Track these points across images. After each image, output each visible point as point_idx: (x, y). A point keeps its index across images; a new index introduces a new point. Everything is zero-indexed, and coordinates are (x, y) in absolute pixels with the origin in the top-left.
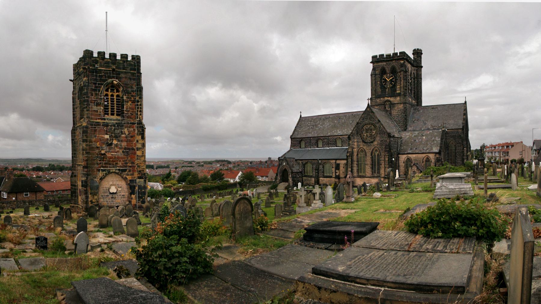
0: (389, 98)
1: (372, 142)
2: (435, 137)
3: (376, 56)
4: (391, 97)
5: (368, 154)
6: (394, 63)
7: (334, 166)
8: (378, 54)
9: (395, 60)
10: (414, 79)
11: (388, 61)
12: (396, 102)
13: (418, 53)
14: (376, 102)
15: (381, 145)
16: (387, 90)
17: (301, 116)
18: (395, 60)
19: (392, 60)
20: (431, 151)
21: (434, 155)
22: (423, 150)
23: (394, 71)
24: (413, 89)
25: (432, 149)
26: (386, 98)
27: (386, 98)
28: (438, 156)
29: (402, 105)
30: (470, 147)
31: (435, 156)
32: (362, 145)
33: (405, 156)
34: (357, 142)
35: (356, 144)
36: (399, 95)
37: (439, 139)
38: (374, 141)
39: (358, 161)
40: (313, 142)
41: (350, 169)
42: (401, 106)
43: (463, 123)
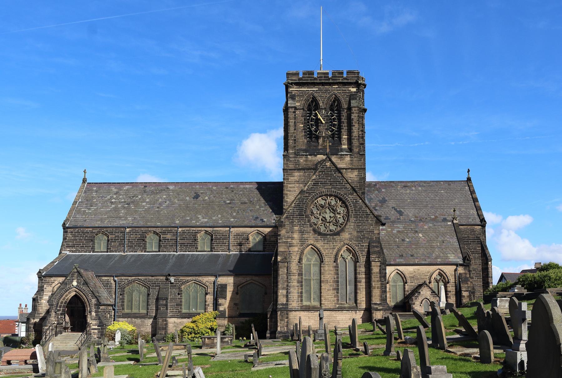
1: (338, 234)
5: (326, 259)
7: (210, 290)
11: (323, 84)
14: (297, 163)
17: (84, 181)
19: (330, 84)
20: (447, 261)
28: (461, 270)
29: (356, 173)
33: (393, 268)
38: (342, 230)
39: (300, 274)
41: (284, 292)
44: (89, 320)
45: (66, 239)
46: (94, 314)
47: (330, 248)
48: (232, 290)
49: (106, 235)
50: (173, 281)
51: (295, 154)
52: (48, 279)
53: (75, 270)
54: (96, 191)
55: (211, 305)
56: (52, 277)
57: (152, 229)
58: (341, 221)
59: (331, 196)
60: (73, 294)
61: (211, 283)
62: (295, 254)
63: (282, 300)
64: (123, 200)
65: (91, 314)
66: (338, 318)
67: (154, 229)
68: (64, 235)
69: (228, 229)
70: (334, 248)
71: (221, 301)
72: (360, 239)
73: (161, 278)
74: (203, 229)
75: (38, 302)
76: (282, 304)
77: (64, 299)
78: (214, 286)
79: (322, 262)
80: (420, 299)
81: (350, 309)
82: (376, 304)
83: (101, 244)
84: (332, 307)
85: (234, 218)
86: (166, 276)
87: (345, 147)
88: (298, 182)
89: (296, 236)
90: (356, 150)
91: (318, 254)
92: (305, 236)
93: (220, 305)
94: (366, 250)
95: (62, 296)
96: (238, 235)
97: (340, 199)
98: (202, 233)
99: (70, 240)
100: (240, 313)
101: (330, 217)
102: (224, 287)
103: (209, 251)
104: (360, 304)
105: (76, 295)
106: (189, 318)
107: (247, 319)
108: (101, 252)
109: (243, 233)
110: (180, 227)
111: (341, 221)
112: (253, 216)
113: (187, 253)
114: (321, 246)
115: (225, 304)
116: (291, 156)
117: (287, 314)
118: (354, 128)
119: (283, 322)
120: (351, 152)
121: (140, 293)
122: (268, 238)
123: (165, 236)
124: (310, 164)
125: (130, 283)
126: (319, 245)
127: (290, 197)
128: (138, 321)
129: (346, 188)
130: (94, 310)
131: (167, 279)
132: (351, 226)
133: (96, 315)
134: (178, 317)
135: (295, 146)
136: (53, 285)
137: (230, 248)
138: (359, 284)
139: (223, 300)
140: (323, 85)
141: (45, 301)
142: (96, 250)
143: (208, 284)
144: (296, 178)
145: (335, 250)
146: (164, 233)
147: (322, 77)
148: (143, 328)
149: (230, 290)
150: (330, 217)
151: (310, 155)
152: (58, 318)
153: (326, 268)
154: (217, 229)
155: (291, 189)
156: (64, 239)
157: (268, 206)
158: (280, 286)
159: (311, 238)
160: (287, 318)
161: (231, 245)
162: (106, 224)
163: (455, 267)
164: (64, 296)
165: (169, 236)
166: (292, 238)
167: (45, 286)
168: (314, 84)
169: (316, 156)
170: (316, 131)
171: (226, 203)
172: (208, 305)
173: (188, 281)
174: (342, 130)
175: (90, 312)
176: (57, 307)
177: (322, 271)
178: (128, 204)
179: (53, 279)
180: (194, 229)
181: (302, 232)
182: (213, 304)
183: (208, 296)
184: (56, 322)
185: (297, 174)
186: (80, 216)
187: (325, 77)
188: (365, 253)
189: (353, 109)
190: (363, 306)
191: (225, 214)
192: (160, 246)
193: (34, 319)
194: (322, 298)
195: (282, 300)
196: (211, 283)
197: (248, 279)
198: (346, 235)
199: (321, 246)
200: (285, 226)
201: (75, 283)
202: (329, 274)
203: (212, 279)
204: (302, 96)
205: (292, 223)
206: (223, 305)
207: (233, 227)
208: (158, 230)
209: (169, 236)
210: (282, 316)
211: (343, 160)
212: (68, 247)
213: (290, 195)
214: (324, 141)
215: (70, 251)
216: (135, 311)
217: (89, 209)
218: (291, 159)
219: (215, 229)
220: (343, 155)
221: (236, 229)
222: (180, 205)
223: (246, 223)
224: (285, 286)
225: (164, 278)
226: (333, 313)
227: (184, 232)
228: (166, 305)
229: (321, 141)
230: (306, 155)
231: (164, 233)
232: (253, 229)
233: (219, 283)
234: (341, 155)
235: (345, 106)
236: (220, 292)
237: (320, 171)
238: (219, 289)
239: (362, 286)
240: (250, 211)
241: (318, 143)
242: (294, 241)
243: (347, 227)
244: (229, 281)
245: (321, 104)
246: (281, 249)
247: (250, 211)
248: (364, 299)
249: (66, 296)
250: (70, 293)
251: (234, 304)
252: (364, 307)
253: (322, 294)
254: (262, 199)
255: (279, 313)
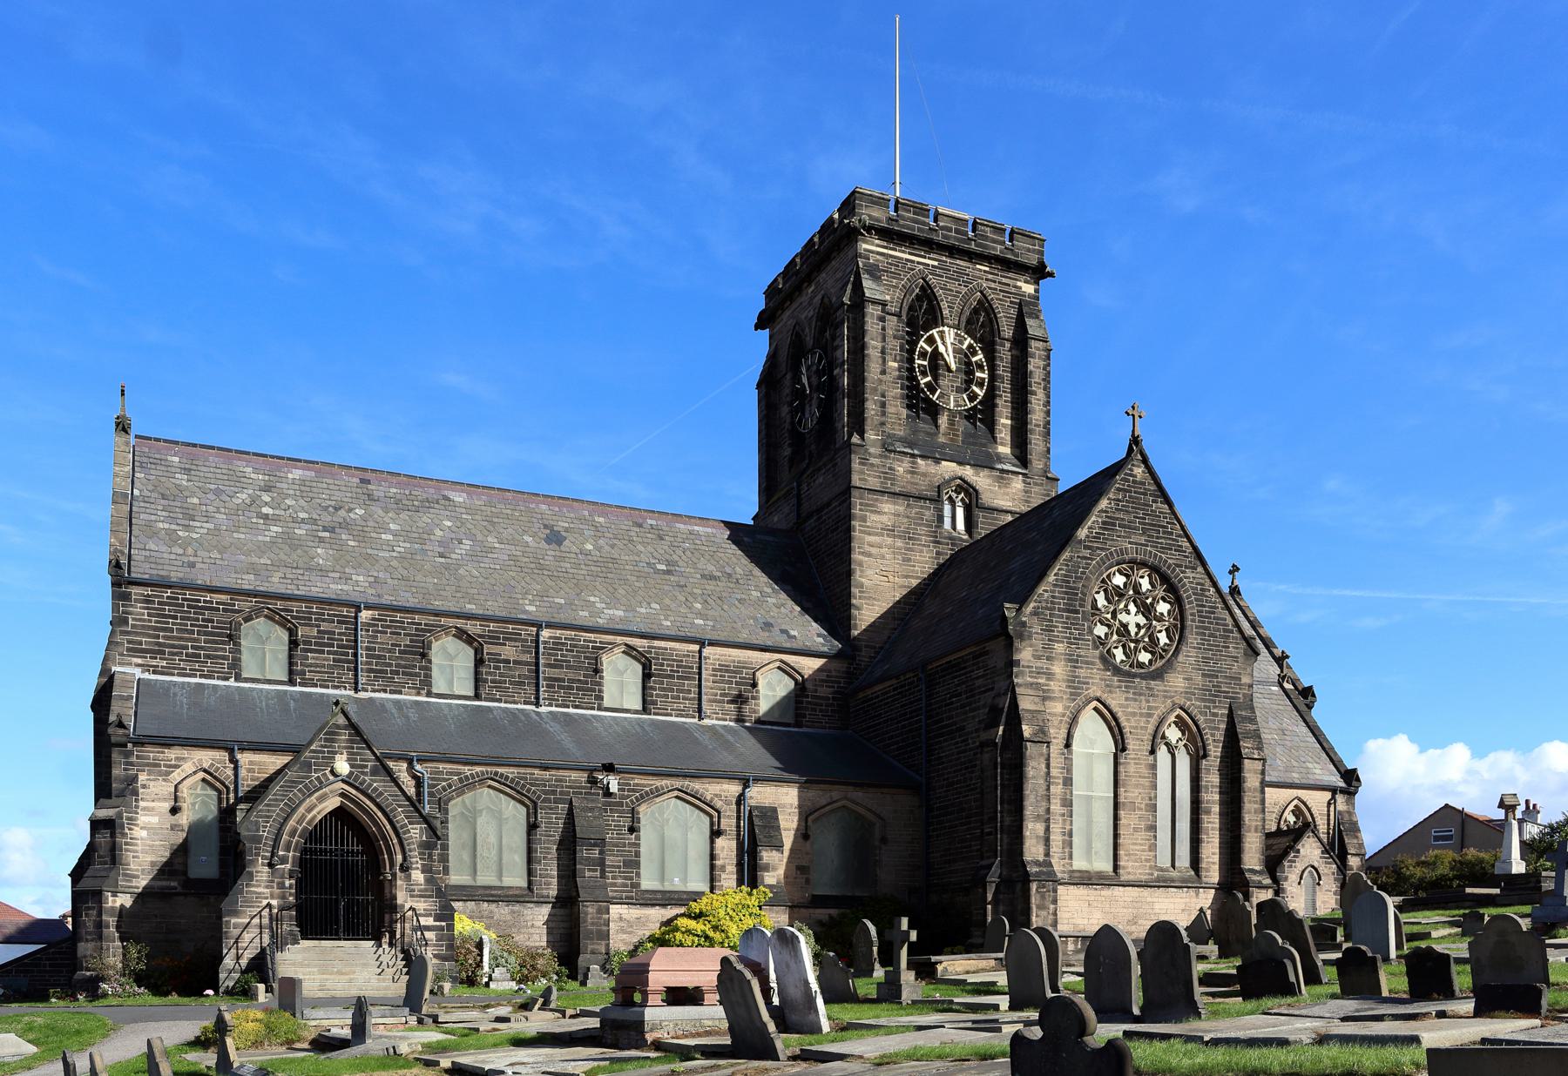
1: (1158, 675)
5: (1131, 744)
7: (728, 823)
11: (953, 251)
14: (889, 474)
19: (972, 256)
44: (401, 897)
45: (125, 621)
46: (418, 876)
47: (1141, 715)
48: (795, 825)
49: (283, 623)
50: (614, 788)
51: (883, 446)
52: (152, 753)
53: (341, 720)
54: (187, 471)
55: (732, 868)
56: (169, 746)
57: (451, 622)
58: (1163, 639)
59: (1143, 564)
60: (333, 803)
61: (728, 803)
62: (1056, 723)
63: (1032, 850)
64: (303, 515)
65: (409, 878)
66: (1157, 906)
67: (460, 623)
68: (115, 608)
69: (697, 647)
70: (1150, 715)
71: (767, 856)
72: (1212, 695)
73: (574, 775)
74: (619, 639)
75: (124, 835)
76: (1037, 863)
77: (299, 822)
78: (738, 811)
79: (1124, 749)
80: (1299, 866)
81: (1183, 884)
82: (1253, 871)
83: (263, 651)
84: (1144, 878)
85: (700, 615)
86: (591, 771)
87: (1005, 450)
88: (891, 531)
89: (1059, 669)
90: (1037, 464)
91: (1110, 729)
92: (1082, 672)
93: (767, 868)
94: (1223, 726)
95: (294, 810)
96: (724, 669)
97: (1165, 579)
98: (617, 650)
99: (144, 630)
100: (814, 896)
101: (1138, 625)
102: (770, 814)
103: (636, 712)
104: (1208, 870)
105: (339, 812)
106: (664, 906)
107: (834, 912)
108: (269, 682)
109: (736, 669)
110: (550, 626)
111: (1163, 639)
112: (755, 619)
113: (571, 710)
114: (1121, 706)
115: (775, 866)
116: (872, 450)
117: (1055, 891)
118: (1032, 399)
119: (1043, 913)
120: (1025, 467)
121: (500, 822)
122: (809, 686)
123: (495, 649)
124: (922, 486)
125: (467, 784)
126: (1116, 701)
127: (869, 572)
128: (502, 911)
129: (1179, 549)
130: (416, 861)
131: (593, 781)
132: (1189, 656)
133: (428, 881)
134: (629, 902)
135: (883, 424)
136: (177, 776)
137: (704, 706)
138: (1204, 817)
139: (775, 853)
140: (951, 256)
141: (144, 833)
142: (245, 675)
143: (719, 804)
144: (884, 519)
145: (1154, 721)
146: (494, 639)
147: (950, 230)
148: (519, 933)
149: (789, 824)
150: (1138, 625)
151: (922, 457)
152: (281, 886)
153: (1132, 769)
154: (662, 644)
155: (874, 551)
156: (118, 621)
157: (783, 596)
158: (1029, 811)
159: (1096, 681)
160: (1055, 901)
161: (704, 697)
162: (275, 584)
163: (1328, 795)
164: (302, 810)
165: (508, 651)
166: (1050, 676)
167: (142, 777)
168: (928, 244)
169: (937, 461)
170: (933, 391)
171: (658, 572)
172: (723, 868)
173: (658, 793)
174: (998, 401)
175: (405, 868)
176: (275, 847)
177: (1122, 776)
178: (332, 530)
179: (172, 754)
180: (592, 636)
181: (1073, 661)
182: (740, 865)
183: (719, 842)
184: (274, 902)
185: (887, 506)
186: (164, 548)
187: (957, 231)
188: (1220, 735)
189: (1033, 344)
190: (1213, 874)
191: (667, 601)
192: (478, 681)
193: (115, 894)
194: (1121, 852)
195: (1033, 850)
196: (728, 803)
197: (835, 795)
198: (1177, 681)
199: (1121, 706)
200: (1030, 637)
201: (342, 766)
202: (1137, 786)
203: (734, 789)
204: (896, 275)
205: (1049, 630)
206: (775, 869)
207: (712, 644)
208: (473, 628)
209: (508, 651)
210: (1043, 897)
211: (1007, 485)
212: (134, 651)
213: (869, 567)
214: (951, 423)
215: (145, 668)
216: (486, 878)
217: (187, 527)
218: (873, 460)
219: (657, 643)
220: (1008, 472)
221: (719, 650)
222: (512, 557)
223: (743, 637)
224: (1042, 811)
225: (582, 777)
226: (1146, 892)
227: (557, 644)
228: (601, 863)
229: (943, 420)
230: (913, 456)
231: (494, 639)
232: (767, 656)
233: (753, 803)
234: (1002, 471)
235: (1007, 331)
236: (755, 834)
237: (1119, 490)
238: (757, 821)
239: (1212, 823)
240: (740, 601)
241: (937, 426)
242: (1054, 685)
243: (1181, 658)
244: (784, 799)
245: (946, 312)
246: (1025, 704)
247: (740, 601)
248: (1216, 858)
249: (309, 810)
250: (321, 799)
251: (799, 868)
252: (1216, 880)
253: (1121, 841)
254: (757, 572)
255: (1034, 886)
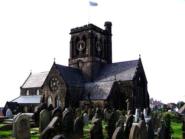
0: (81, 59)
2: (107, 87)
3: (74, 29)
4: (82, 57)
6: (85, 33)
8: (74, 27)
9: (85, 30)
10: (105, 44)
11: (81, 31)
12: (85, 61)
13: (108, 25)
15: (61, 92)
16: (80, 52)
18: (85, 30)
21: (103, 101)
22: (96, 97)
23: (84, 38)
24: (103, 51)
25: (103, 97)
26: (79, 59)
27: (79, 59)
30: (149, 96)
31: (104, 102)
32: (49, 92)
34: (47, 90)
35: (46, 92)
36: (87, 56)
37: (110, 89)
40: (34, 91)
42: (88, 64)
43: (134, 76)
